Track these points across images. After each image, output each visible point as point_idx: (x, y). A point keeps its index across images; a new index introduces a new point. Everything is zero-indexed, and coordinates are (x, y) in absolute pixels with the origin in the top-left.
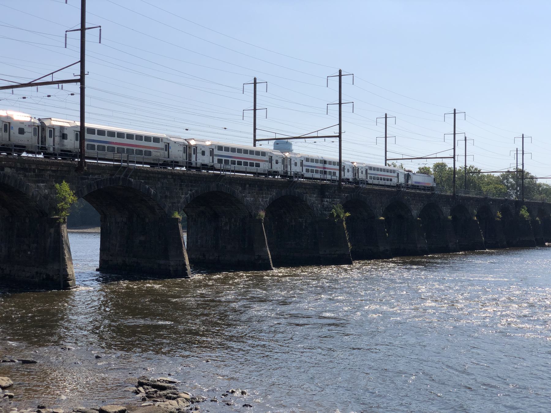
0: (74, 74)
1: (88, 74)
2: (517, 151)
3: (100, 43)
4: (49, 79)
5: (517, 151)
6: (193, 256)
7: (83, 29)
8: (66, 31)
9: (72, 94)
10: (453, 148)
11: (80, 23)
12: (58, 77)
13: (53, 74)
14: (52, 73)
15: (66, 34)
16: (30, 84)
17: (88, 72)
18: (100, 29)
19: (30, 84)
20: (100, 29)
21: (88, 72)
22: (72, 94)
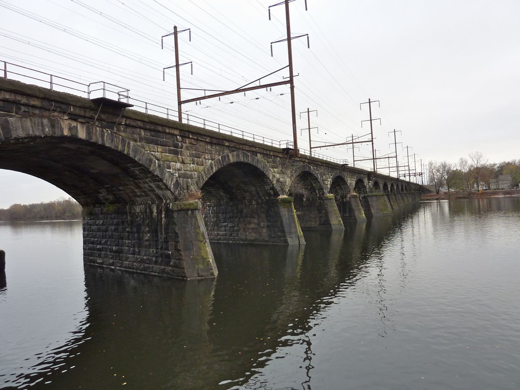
0: (283, 77)
1: (298, 75)
2: (352, 137)
3: (164, 81)
4: (257, 84)
5: (352, 137)
6: (303, 225)
7: (177, 66)
8: (271, 43)
9: (231, 103)
10: (371, 132)
11: (287, 33)
12: (263, 82)
13: (260, 80)
14: (259, 79)
15: (271, 45)
16: (237, 91)
17: (298, 74)
18: (308, 37)
19: (237, 91)
20: (308, 37)
21: (298, 74)
22: (231, 103)
